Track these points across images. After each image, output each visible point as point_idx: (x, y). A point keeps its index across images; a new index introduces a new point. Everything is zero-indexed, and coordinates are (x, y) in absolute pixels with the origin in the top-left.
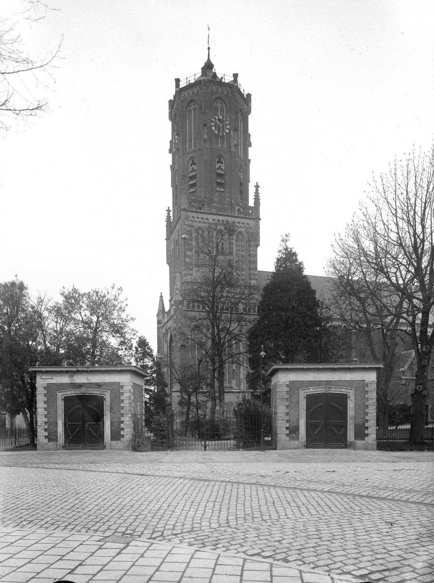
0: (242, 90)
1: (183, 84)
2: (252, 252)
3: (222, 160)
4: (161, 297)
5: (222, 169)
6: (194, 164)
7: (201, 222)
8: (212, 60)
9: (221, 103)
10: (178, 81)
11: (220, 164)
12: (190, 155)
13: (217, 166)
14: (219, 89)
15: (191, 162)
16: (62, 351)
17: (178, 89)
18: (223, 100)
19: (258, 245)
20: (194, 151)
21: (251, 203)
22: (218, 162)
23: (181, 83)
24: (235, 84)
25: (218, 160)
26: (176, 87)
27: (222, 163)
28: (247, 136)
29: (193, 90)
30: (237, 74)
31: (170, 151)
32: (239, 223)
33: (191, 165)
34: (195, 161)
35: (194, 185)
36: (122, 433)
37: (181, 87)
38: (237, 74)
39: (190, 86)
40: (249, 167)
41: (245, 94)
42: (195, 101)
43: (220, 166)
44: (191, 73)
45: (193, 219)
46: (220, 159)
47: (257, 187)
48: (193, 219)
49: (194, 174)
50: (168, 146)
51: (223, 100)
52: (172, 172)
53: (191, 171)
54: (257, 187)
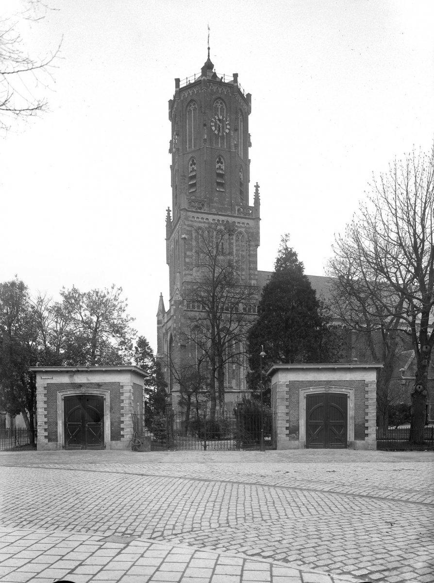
0: (242, 90)
1: (183, 84)
2: (252, 252)
3: (222, 160)
4: (161, 297)
5: (222, 169)
6: (194, 164)
7: (201, 222)
8: (212, 60)
9: (221, 103)
10: (178, 81)
11: (220, 164)
12: (190, 155)
13: (217, 166)
14: (219, 89)
15: (191, 162)
16: (62, 351)
17: (178, 89)
18: (223, 100)
19: (258, 245)
20: (194, 151)
21: (251, 203)
22: (218, 162)
23: (181, 83)
24: (235, 84)
25: (218, 160)
26: (176, 87)
27: (222, 163)
28: (247, 136)
29: (193, 90)
30: (237, 74)
31: (170, 151)
32: (239, 223)
33: (191, 165)
34: (195, 161)
35: (194, 185)
36: (122, 433)
37: (181, 87)
38: (237, 74)
39: (190, 86)
40: (249, 167)
41: (245, 94)
42: (195, 101)
43: (220, 166)
44: (191, 73)
45: (193, 219)
46: (220, 159)
47: (257, 187)
48: (193, 219)
49: (194, 174)
50: (168, 146)
51: (223, 100)
52: (172, 172)
53: (191, 171)
54: (257, 187)
